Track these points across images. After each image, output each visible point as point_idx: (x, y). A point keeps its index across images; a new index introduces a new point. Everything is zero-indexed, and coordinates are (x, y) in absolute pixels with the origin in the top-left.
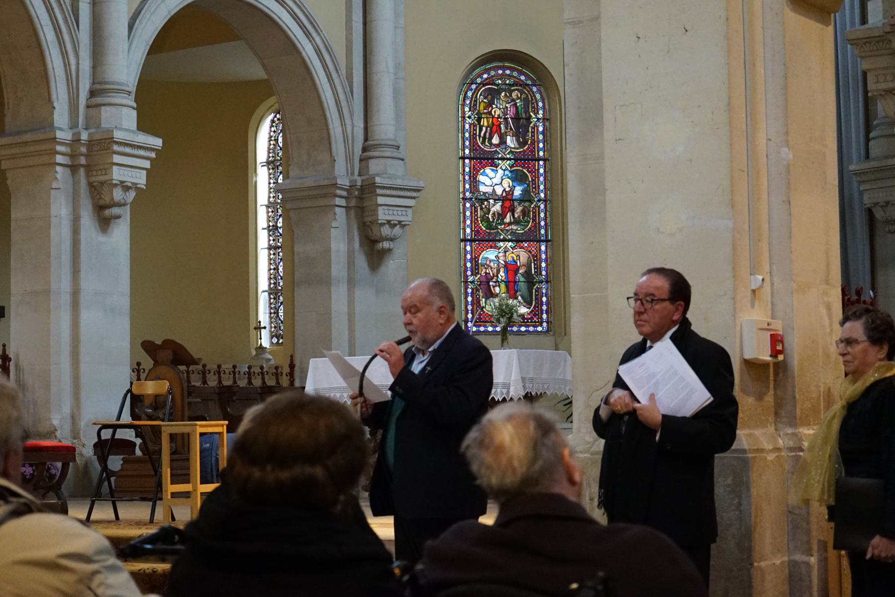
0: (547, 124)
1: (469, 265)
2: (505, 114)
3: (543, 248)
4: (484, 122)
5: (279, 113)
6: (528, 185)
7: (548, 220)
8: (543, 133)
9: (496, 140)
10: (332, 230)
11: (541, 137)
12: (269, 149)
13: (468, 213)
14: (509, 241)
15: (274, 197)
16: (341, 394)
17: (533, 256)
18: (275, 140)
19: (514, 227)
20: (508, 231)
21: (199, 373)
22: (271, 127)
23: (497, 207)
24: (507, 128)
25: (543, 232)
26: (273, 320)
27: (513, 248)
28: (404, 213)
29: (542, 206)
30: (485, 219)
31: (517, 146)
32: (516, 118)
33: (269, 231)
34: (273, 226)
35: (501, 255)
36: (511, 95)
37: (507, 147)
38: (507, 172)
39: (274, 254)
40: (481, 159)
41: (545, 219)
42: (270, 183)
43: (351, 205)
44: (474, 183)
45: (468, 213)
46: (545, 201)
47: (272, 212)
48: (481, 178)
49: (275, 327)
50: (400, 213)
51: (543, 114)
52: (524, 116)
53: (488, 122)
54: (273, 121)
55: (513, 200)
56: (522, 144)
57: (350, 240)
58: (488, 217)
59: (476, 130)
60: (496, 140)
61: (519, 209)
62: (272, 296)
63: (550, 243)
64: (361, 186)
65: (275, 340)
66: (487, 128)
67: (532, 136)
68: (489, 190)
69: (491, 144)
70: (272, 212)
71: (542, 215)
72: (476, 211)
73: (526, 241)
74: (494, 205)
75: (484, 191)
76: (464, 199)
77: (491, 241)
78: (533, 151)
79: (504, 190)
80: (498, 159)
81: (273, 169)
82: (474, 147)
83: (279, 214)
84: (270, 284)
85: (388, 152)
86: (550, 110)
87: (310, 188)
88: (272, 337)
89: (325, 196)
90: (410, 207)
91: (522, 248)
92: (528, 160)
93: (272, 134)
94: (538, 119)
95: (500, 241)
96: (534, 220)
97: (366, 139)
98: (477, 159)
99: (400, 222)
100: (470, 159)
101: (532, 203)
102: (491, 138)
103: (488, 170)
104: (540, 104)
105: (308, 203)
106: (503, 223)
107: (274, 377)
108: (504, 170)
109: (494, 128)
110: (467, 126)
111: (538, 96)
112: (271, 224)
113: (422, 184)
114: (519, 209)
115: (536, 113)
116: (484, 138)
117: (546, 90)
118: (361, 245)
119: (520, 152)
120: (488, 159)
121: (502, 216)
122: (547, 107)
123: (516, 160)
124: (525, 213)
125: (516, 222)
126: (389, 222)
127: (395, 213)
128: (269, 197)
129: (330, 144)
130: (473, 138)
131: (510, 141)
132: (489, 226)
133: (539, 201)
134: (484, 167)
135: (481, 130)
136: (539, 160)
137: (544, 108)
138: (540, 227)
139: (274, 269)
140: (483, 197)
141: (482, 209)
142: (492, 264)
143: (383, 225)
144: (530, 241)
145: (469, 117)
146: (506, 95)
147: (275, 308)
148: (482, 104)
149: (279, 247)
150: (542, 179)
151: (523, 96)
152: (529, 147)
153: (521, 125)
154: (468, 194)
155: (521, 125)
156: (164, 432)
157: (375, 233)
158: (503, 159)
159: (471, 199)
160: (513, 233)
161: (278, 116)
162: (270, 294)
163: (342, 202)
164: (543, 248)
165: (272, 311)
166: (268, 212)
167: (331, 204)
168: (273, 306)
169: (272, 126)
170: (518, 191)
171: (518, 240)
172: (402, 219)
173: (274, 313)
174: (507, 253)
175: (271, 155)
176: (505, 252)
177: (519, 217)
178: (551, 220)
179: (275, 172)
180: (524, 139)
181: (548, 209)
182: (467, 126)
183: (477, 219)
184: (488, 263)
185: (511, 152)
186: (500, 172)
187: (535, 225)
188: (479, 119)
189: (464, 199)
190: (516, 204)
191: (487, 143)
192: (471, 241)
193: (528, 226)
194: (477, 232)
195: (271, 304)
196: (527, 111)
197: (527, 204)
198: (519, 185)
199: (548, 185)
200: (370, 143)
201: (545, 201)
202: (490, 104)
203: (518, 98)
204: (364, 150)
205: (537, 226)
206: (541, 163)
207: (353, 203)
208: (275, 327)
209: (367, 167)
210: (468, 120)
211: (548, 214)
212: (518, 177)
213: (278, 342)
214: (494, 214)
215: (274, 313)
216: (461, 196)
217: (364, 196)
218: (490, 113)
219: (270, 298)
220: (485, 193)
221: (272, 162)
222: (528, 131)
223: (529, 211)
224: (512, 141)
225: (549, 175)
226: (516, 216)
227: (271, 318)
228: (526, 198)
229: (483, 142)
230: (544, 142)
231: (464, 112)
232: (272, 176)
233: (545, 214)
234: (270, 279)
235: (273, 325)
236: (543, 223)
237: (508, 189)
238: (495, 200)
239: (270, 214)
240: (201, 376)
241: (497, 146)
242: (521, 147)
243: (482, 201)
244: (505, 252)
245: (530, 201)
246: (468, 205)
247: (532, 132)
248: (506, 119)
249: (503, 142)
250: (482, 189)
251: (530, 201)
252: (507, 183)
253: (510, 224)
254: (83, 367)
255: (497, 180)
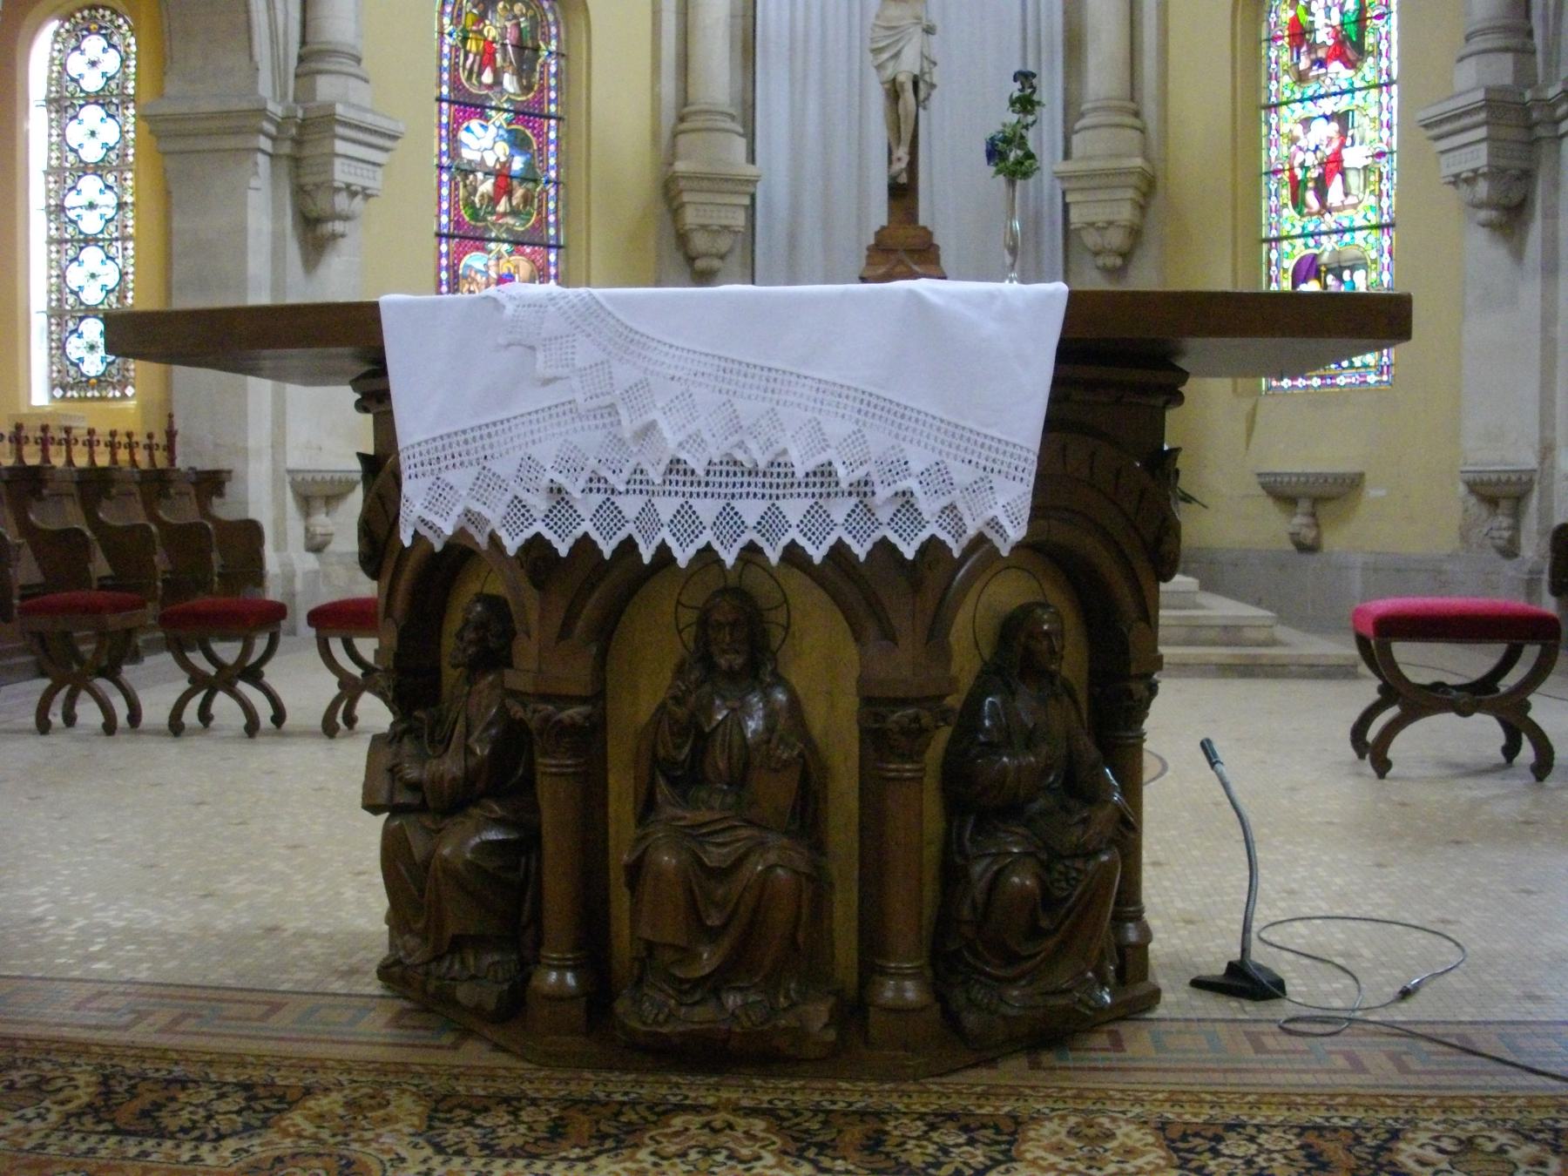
0: (563, 62)
1: (444, 275)
2: (504, 38)
3: (552, 257)
4: (472, 45)
5: (69, 20)
6: (533, 156)
7: (561, 214)
8: (556, 75)
9: (487, 77)
10: (251, 193)
11: (553, 82)
12: (50, 79)
13: (445, 191)
14: (504, 241)
15: (58, 158)
16: (766, 504)
17: (539, 270)
18: (61, 64)
19: (510, 220)
20: (501, 225)
21: (36, 443)
22: (53, 43)
23: (487, 186)
24: (504, 60)
25: (552, 231)
26: (55, 360)
27: (510, 254)
28: (371, 174)
29: (552, 192)
30: (470, 204)
31: (518, 92)
32: (519, 47)
33: (49, 213)
34: (57, 205)
35: (492, 263)
36: (512, 9)
37: (503, 92)
38: (501, 132)
39: (58, 252)
40: (466, 105)
41: (556, 211)
42: (50, 135)
43: (281, 152)
44: (455, 145)
45: (445, 191)
46: (557, 183)
47: (56, 182)
48: (463, 136)
49: (59, 371)
50: (365, 173)
51: (557, 47)
52: (530, 44)
53: (478, 46)
54: (57, 34)
55: (512, 177)
56: (526, 89)
57: (277, 216)
58: (473, 202)
59: (457, 57)
60: (487, 77)
61: (519, 193)
62: (53, 321)
63: (562, 251)
64: (303, 120)
65: (58, 393)
66: (475, 55)
67: (541, 79)
68: (476, 157)
69: (480, 83)
70: (56, 182)
71: (552, 205)
72: (457, 189)
73: (529, 244)
74: (483, 182)
75: (471, 158)
76: (441, 167)
77: (478, 240)
78: (540, 102)
79: (498, 159)
80: (492, 108)
81: (57, 112)
82: (455, 84)
83: (67, 186)
84: (50, 300)
85: (350, 66)
86: (567, 41)
87: (211, 116)
88: (53, 387)
89: (237, 132)
90: (379, 165)
91: (522, 254)
92: (536, 116)
93: (55, 54)
94: (550, 53)
95: (491, 240)
96: (539, 213)
97: (303, 42)
98: (460, 104)
99: (364, 189)
100: (451, 102)
101: (537, 185)
102: (480, 74)
103: (475, 124)
104: (553, 30)
105: (205, 144)
106: (493, 212)
107: (86, 449)
108: (499, 128)
109: (487, 57)
110: (446, 49)
111: (551, 17)
112: (53, 202)
113: (401, 127)
114: (519, 193)
115: (548, 43)
116: (471, 72)
117: (563, 7)
118: (295, 226)
119: (522, 102)
120: (477, 106)
121: (493, 200)
122: (563, 36)
123: (517, 113)
124: (527, 200)
125: (514, 212)
126: (348, 186)
127: (359, 171)
128: (50, 158)
129: (250, 39)
130: (454, 68)
131: (509, 82)
132: (475, 215)
133: (548, 182)
134: (470, 118)
135: (466, 58)
136: (549, 117)
137: (558, 36)
138: (548, 224)
139: (58, 276)
140: (467, 167)
141: (465, 186)
142: (478, 277)
143: (338, 190)
144: (533, 244)
145: (450, 35)
146: (505, 7)
147: (59, 340)
148: (470, 16)
149: (66, 241)
150: (552, 148)
151: (530, 13)
152: (534, 97)
153: (525, 54)
154: (445, 160)
155: (525, 54)
156: (1156, 864)
157: (320, 204)
158: (498, 109)
159: (449, 168)
160: (509, 230)
161: (67, 25)
162: (49, 317)
163: (265, 143)
164: (552, 257)
165: (54, 345)
166: (48, 182)
167: (250, 145)
168: (55, 337)
169: (56, 41)
170: (518, 164)
171: (517, 243)
172: (367, 183)
173: (58, 348)
174: (501, 262)
175: (53, 89)
176: (498, 259)
177: (518, 205)
178: (567, 215)
179: (61, 117)
180: (529, 81)
181: (561, 197)
182: (446, 49)
183: (457, 202)
184: (473, 274)
185: (508, 100)
186: (492, 130)
187: (541, 220)
188: (465, 39)
189: (441, 167)
190: (515, 183)
191: (474, 81)
192: (449, 237)
193: (529, 220)
194: (458, 224)
195: (51, 333)
196: (534, 38)
197: (530, 185)
198: (521, 154)
199: (563, 158)
200: (308, 47)
201: (557, 183)
202: (481, 18)
203: (522, 15)
204: (301, 59)
205: (543, 223)
206: (553, 122)
207: (286, 148)
208: (59, 371)
209: (312, 90)
210: (448, 40)
211: (560, 203)
212: (518, 142)
213: (63, 397)
214: (482, 196)
215: (58, 348)
216: (436, 161)
217: (306, 138)
218: (480, 32)
219: (50, 324)
220: (470, 162)
221: (56, 100)
222: (535, 70)
223: (533, 197)
224: (511, 83)
225: (563, 143)
226: (514, 203)
227: (51, 356)
228: (529, 176)
229: (469, 78)
230: (558, 89)
231: (441, 26)
232: (54, 124)
233: (557, 203)
234: (50, 292)
235: (55, 368)
236: (552, 218)
237: (503, 159)
238: (486, 174)
239: (52, 186)
240: (39, 447)
241: (490, 87)
242: (523, 94)
243: (466, 173)
244: (498, 259)
245: (536, 181)
246: (445, 177)
247: (542, 73)
248: (504, 45)
249: (498, 82)
250: (466, 154)
251: (536, 181)
252: (502, 149)
253: (504, 214)
254: (1532, 388)
255: (488, 143)
